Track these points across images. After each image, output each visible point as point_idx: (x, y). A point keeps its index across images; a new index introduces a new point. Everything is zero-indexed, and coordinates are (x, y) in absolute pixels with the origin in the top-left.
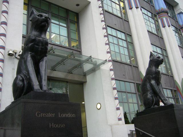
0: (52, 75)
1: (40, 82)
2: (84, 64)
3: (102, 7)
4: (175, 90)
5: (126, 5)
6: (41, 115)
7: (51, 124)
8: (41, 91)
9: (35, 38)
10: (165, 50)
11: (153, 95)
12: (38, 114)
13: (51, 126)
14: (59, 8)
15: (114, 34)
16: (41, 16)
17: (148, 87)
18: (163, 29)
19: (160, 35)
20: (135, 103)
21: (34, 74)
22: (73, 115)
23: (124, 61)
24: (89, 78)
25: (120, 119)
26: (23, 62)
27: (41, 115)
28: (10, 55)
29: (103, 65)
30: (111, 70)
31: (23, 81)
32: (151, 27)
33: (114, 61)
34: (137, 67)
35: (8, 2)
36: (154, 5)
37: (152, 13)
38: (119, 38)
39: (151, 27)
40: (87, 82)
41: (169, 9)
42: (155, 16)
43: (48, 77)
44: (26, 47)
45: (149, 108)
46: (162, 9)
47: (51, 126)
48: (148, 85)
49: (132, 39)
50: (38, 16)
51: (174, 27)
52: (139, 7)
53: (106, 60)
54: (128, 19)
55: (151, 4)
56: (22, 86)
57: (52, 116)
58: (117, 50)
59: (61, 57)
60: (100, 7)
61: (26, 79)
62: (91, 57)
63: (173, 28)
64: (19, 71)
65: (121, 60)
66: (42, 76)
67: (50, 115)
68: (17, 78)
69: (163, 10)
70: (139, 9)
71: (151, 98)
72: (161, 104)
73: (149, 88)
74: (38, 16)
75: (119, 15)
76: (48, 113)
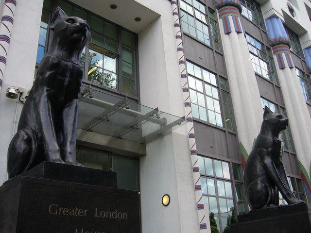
0: (84, 139)
1: (62, 146)
2: (143, 122)
3: (180, 26)
4: (300, 180)
5: (220, 27)
6: (58, 211)
8: (63, 163)
9: (59, 61)
10: (284, 109)
11: (267, 184)
12: (53, 210)
14: (104, 23)
16: (73, 21)
17: (258, 170)
18: (280, 72)
19: (275, 83)
21: (52, 128)
22: (124, 215)
23: (212, 122)
24: (150, 148)
25: (203, 226)
26: (32, 106)
27: (58, 211)
28: (10, 95)
29: (178, 125)
30: (191, 136)
31: (28, 141)
33: (197, 122)
35: (15, 3)
36: (266, 30)
37: (263, 44)
40: (147, 156)
41: (291, 39)
42: (268, 49)
43: (78, 141)
44: (41, 77)
45: (258, 208)
48: (259, 167)
50: (68, 21)
51: (299, 69)
52: (242, 31)
53: (184, 118)
54: (222, 51)
55: (261, 29)
57: (81, 214)
58: (202, 103)
59: (103, 107)
60: (176, 25)
61: (34, 139)
62: (157, 109)
63: (297, 72)
64: (23, 123)
65: (208, 119)
66: (67, 135)
67: (78, 211)
68: (17, 137)
69: (281, 40)
70: (242, 35)
71: (264, 191)
72: (282, 202)
73: (261, 171)
74: (68, 21)
75: (208, 43)
76: (74, 208)
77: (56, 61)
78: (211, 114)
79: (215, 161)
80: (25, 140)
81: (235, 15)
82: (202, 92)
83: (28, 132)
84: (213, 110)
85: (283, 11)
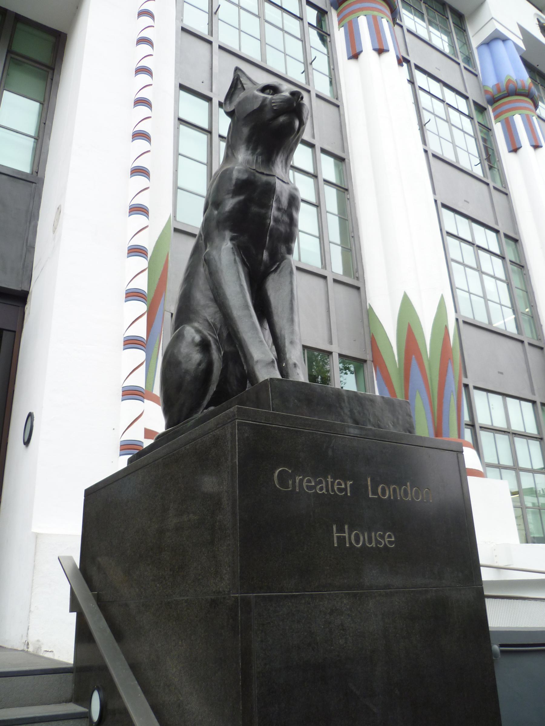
7: (341, 530)
13: (341, 540)
15: (466, 235)
34: (358, 288)
38: (479, 247)
46: (509, 81)
47: (341, 540)
56: (203, 366)
57: (340, 490)
67: (333, 483)
70: (391, 57)
76: (326, 478)
79: (509, 400)
81: (375, 13)
85: (523, 31)
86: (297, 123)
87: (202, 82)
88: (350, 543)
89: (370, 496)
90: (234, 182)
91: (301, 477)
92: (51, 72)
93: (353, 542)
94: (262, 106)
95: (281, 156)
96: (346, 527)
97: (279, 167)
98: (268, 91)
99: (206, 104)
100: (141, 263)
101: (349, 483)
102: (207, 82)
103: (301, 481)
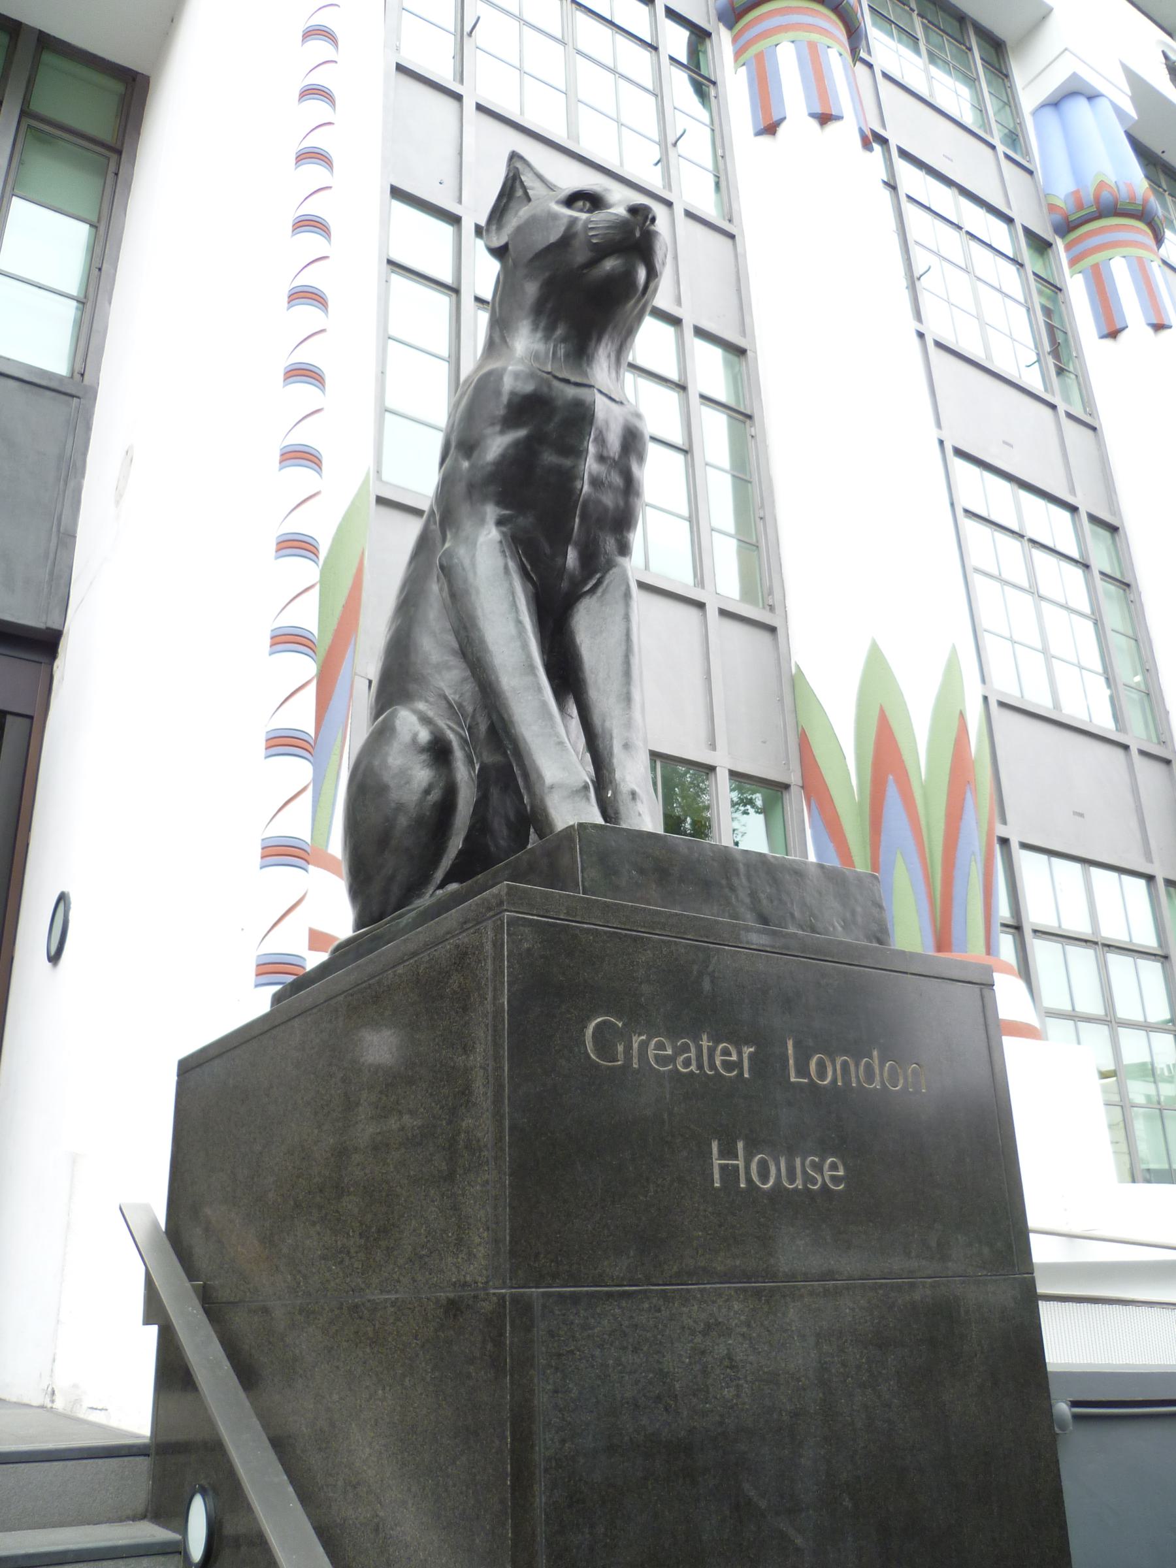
7: (728, 1151)
13: (730, 1174)
20: (1089, 1019)
32: (979, 318)
39: (979, 318)
46: (1102, 185)
47: (730, 1174)
49: (1121, 553)
54: (1092, 411)
56: (435, 796)
57: (728, 1066)
67: (712, 1051)
69: (1105, 195)
70: (846, 132)
76: (696, 1038)
77: (529, 388)
78: (1066, 675)
79: (1094, 871)
80: (423, 750)
81: (815, 37)
82: (1026, 585)
83: (431, 714)
84: (1076, 662)
85: (1133, 79)
86: (642, 274)
87: (441, 183)
88: (749, 1180)
89: (792, 1080)
90: (505, 399)
91: (644, 1037)
92: (114, 157)
93: (755, 1178)
94: (566, 240)
95: (607, 345)
96: (740, 1145)
97: (602, 369)
98: (580, 204)
99: (447, 229)
100: (305, 571)
101: (748, 1050)
102: (451, 182)
103: (644, 1046)
